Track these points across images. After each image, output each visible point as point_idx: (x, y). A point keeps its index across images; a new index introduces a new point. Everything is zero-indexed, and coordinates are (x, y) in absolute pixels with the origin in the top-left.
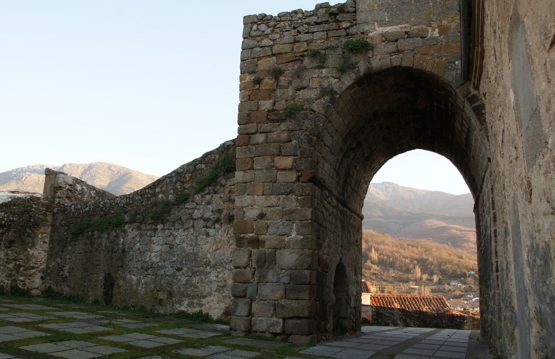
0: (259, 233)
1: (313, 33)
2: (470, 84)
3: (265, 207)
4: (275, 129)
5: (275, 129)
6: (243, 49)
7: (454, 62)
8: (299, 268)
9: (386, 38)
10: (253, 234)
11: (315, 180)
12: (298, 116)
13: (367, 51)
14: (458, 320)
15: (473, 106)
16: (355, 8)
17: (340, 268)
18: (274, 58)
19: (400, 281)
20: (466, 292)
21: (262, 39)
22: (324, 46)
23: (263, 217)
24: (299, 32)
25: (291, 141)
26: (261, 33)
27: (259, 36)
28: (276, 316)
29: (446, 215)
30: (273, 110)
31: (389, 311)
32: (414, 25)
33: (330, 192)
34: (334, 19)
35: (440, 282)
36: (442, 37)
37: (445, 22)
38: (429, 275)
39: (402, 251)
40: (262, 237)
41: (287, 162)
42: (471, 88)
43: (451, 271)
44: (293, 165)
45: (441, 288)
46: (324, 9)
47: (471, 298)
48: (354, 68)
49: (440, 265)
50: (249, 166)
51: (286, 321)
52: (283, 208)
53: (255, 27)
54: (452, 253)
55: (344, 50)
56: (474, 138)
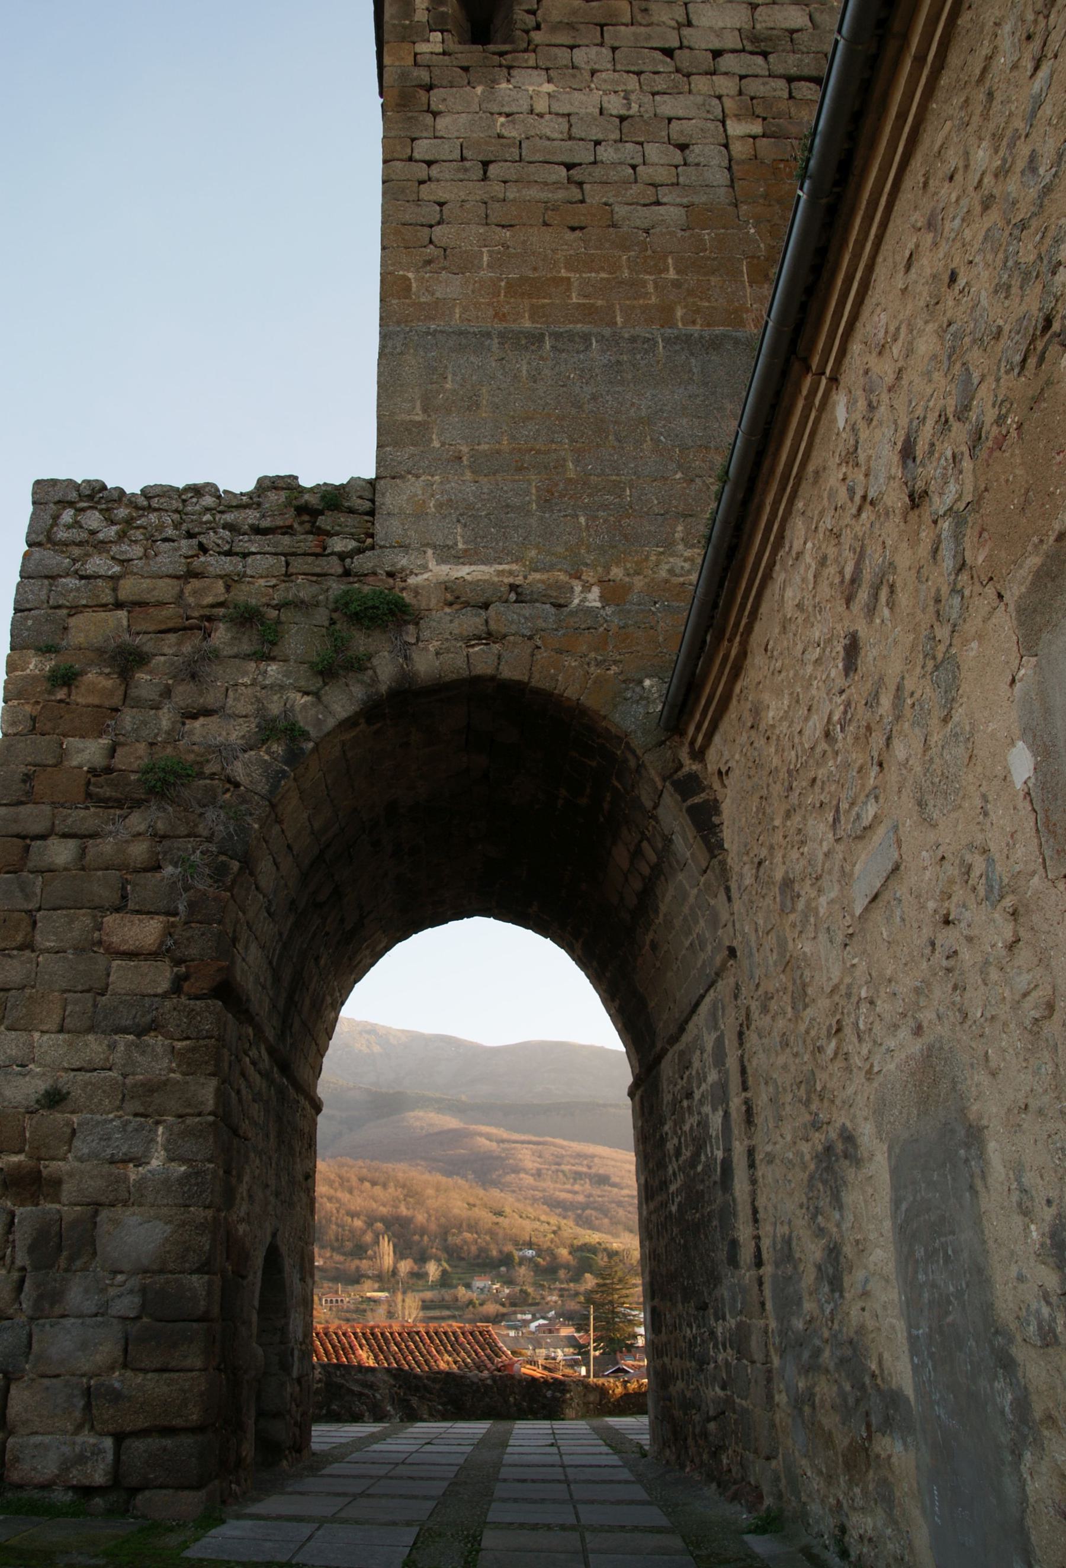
0: (43, 1153)
1: (245, 555)
2: (682, 744)
3: (66, 1070)
4: (111, 827)
5: (111, 827)
6: (25, 575)
7: (640, 682)
8: (171, 1266)
9: (456, 596)
10: (21, 1157)
11: (225, 991)
12: (186, 793)
13: (401, 624)
14: (549, 1394)
15: (689, 802)
16: (373, 501)
17: (273, 1257)
18: (122, 614)
19: (335, 1279)
20: (513, 1304)
21: (88, 555)
22: (277, 597)
23: (57, 1102)
24: (203, 549)
25: (158, 868)
26: (84, 535)
27: (80, 544)
28: (92, 1428)
29: (464, 1098)
30: (108, 770)
31: (359, 1376)
32: (536, 570)
33: (259, 1030)
34: (307, 526)
35: (445, 1281)
36: (609, 610)
37: (617, 573)
38: (415, 1261)
39: (344, 1196)
40: (51, 1168)
41: (146, 931)
42: (684, 755)
43: (474, 1249)
44: (162, 943)
45: (447, 1297)
46: (283, 494)
47: (526, 1323)
48: (362, 669)
49: (446, 1233)
50: (19, 938)
51: (127, 1442)
52: (125, 1076)
53: (67, 516)
54: (478, 1202)
55: (335, 616)
56: (671, 892)
